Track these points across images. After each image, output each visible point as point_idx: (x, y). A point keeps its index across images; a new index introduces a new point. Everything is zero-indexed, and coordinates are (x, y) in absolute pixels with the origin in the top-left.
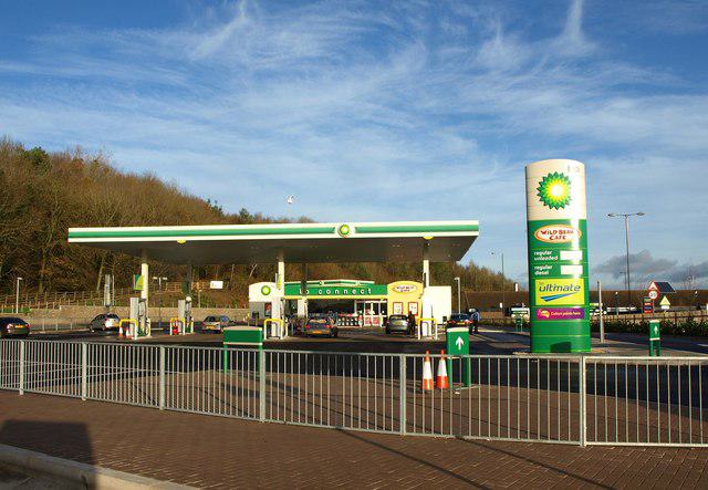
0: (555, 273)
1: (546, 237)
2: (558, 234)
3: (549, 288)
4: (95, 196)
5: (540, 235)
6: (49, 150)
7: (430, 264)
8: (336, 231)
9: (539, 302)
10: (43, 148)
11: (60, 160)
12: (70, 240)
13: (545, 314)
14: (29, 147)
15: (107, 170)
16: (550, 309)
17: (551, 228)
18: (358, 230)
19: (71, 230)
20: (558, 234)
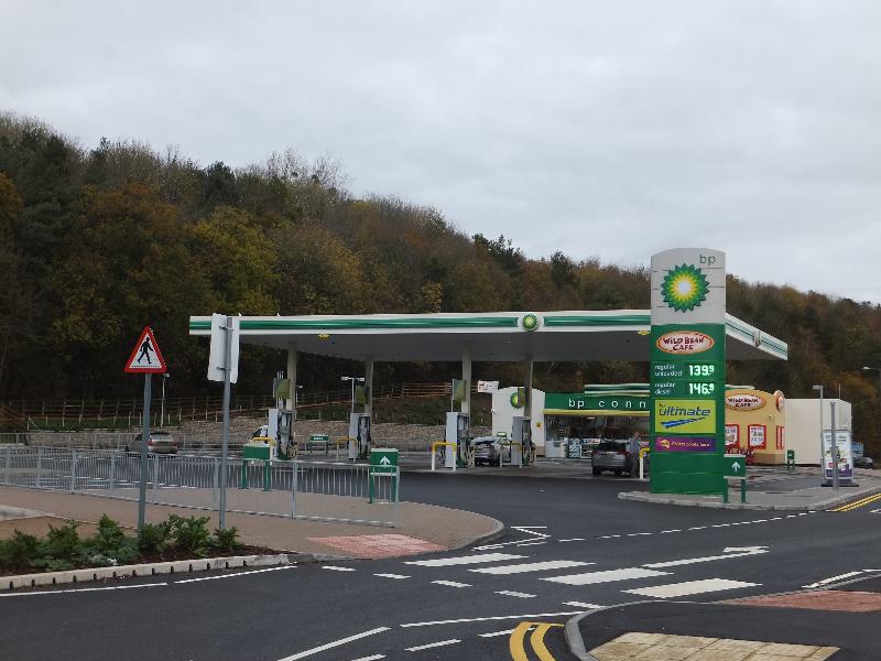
0: (681, 392)
1: (670, 347)
2: (683, 343)
3: (670, 411)
4: (259, 250)
5: (662, 343)
6: (237, 163)
7: (782, 360)
8: (519, 323)
9: (659, 428)
10: (226, 164)
11: (251, 181)
12: (192, 332)
13: (665, 443)
14: (204, 163)
15: (333, 191)
16: (670, 437)
17: (676, 336)
18: (548, 323)
19: (193, 319)
20: (683, 343)
